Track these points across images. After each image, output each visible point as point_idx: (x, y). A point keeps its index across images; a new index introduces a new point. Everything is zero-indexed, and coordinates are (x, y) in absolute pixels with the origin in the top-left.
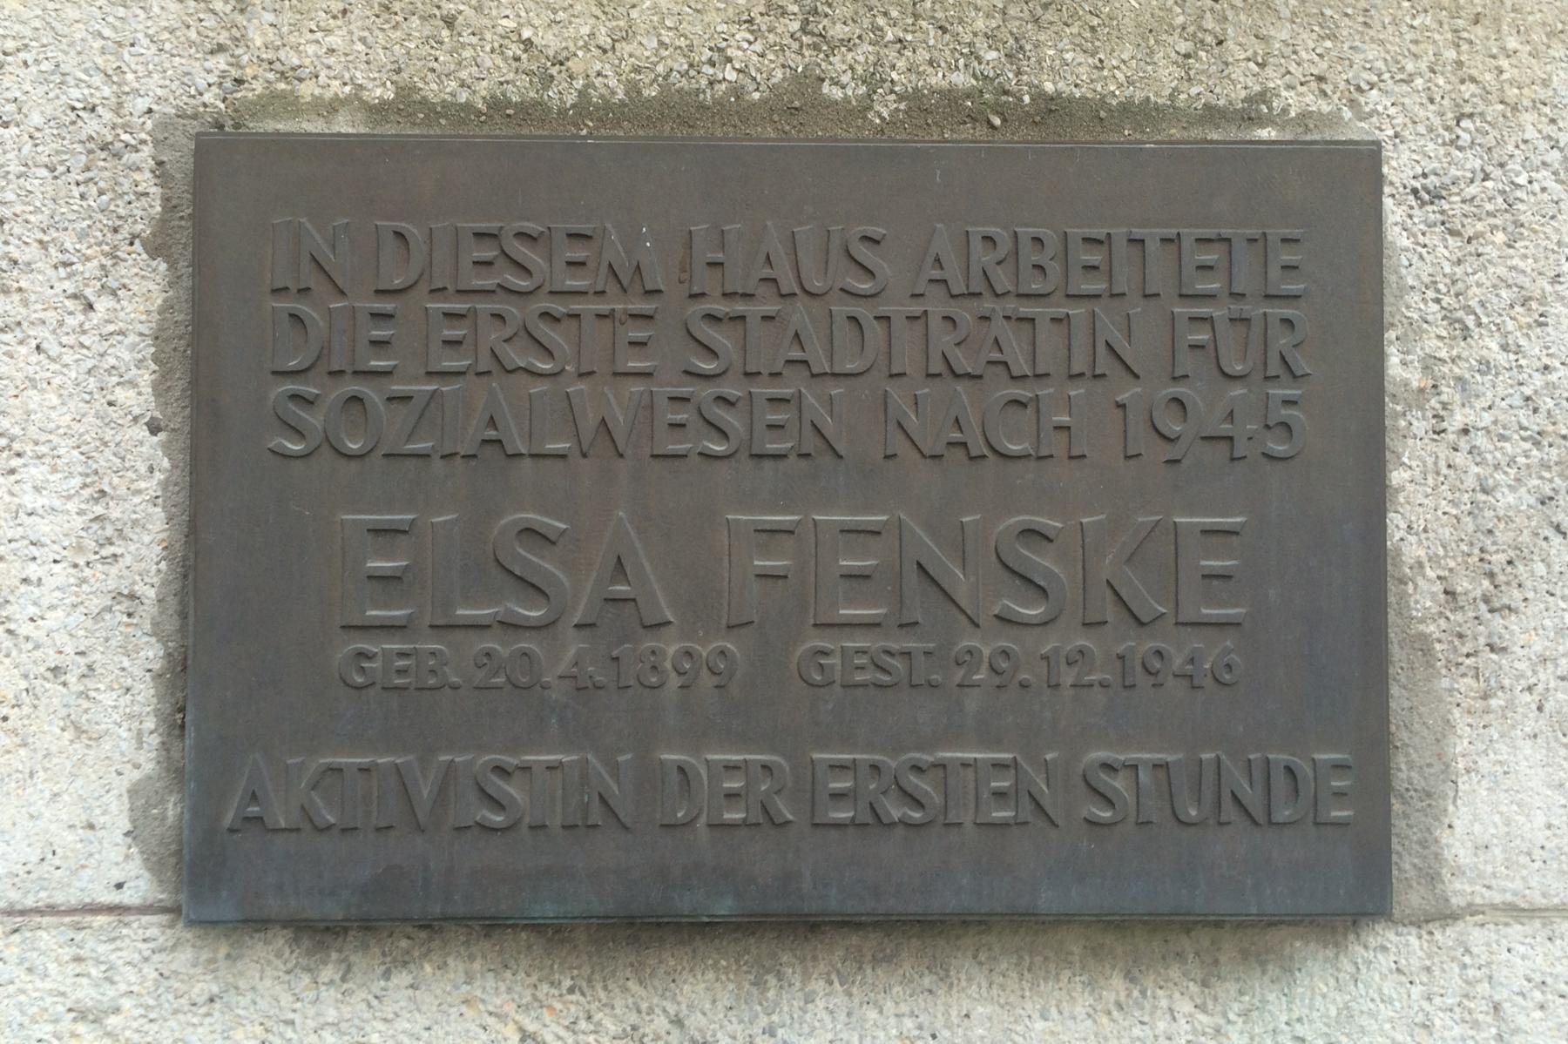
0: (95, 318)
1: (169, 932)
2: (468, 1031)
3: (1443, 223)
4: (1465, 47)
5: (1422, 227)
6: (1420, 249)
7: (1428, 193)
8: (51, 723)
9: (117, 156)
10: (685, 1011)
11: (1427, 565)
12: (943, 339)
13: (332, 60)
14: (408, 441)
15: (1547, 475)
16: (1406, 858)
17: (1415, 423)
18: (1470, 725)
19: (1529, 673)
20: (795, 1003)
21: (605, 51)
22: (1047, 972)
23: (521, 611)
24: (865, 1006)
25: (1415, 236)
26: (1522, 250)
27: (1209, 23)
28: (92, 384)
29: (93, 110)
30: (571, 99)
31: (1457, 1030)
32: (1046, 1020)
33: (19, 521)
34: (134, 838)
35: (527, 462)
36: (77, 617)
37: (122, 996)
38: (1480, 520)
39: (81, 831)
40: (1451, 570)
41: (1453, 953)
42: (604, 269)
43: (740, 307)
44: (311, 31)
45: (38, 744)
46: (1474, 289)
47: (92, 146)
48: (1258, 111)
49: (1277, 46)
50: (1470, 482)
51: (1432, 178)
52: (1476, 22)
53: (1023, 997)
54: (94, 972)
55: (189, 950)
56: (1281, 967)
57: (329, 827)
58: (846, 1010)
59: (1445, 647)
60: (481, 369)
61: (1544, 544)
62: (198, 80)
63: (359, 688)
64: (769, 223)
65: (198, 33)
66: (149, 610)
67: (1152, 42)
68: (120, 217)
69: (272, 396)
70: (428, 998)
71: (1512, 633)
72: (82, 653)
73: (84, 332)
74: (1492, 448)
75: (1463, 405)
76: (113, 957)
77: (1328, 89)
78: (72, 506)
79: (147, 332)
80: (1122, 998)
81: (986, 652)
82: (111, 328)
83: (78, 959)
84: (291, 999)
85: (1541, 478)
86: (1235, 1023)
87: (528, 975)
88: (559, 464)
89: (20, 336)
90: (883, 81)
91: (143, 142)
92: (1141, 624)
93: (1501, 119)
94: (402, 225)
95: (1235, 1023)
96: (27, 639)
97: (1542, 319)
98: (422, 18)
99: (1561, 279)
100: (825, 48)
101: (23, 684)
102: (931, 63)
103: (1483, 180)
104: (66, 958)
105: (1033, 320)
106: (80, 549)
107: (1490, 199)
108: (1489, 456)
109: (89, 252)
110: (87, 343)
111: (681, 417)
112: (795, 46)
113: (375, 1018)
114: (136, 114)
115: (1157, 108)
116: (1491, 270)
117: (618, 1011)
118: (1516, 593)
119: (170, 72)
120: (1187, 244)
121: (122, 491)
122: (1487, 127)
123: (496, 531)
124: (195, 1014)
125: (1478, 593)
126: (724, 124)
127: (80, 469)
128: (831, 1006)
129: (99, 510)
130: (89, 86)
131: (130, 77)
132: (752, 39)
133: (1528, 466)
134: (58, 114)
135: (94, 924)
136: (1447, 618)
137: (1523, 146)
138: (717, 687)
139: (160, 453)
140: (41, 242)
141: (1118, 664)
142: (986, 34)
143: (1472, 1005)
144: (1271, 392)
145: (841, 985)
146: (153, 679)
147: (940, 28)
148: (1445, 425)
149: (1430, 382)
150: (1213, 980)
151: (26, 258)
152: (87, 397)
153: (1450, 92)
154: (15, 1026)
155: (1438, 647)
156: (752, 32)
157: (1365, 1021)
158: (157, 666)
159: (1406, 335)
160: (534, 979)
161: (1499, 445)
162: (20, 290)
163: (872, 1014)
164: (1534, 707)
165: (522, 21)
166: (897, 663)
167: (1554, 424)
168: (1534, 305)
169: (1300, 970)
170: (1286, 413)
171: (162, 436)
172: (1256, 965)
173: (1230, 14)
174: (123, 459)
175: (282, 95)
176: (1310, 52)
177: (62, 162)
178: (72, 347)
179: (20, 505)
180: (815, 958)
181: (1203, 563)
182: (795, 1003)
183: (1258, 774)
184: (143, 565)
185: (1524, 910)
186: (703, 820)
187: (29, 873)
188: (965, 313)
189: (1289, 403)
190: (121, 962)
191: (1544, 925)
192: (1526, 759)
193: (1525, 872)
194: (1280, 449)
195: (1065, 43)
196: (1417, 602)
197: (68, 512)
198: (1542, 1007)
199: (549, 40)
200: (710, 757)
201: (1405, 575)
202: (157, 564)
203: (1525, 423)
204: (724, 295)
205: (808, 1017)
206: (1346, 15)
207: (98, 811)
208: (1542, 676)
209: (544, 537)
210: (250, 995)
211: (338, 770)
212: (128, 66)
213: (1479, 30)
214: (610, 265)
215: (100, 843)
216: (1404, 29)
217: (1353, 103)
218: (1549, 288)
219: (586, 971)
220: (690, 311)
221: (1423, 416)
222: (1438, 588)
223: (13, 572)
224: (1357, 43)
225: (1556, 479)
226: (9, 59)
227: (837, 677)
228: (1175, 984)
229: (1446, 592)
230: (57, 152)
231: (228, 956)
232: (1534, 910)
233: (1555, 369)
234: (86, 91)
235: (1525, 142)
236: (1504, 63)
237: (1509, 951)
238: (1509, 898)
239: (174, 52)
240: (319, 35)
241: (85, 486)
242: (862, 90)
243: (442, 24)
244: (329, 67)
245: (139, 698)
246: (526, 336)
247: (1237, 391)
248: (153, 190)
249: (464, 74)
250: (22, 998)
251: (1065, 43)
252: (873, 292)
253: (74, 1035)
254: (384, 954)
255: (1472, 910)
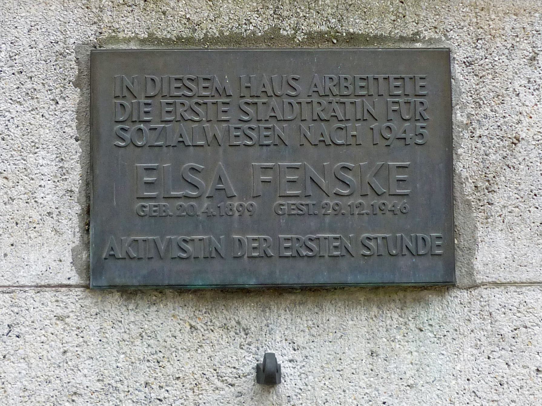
0: (59, 106)
1: (84, 293)
2: (174, 324)
3: (473, 72)
4: (479, 18)
5: (466, 73)
6: (466, 80)
7: (468, 63)
8: (48, 229)
9: (65, 57)
10: (241, 319)
11: (469, 178)
12: (318, 109)
13: (128, 26)
14: (156, 142)
15: (505, 150)
16: (463, 269)
17: (465, 134)
18: (482, 227)
19: (500, 211)
20: (275, 317)
21: (212, 21)
22: (353, 306)
23: (191, 193)
24: (297, 318)
25: (464, 76)
26: (497, 81)
27: (401, 10)
28: (58, 126)
29: (57, 43)
30: (202, 36)
31: (478, 321)
32: (353, 321)
33: (38, 168)
34: (73, 264)
35: (192, 148)
36: (55, 197)
37: (70, 312)
38: (485, 164)
39: (57, 262)
40: (476, 180)
41: (478, 297)
42: (214, 89)
43: (256, 100)
44: (122, 17)
45: (45, 235)
46: (482, 92)
47: (58, 54)
48: (416, 38)
49: (422, 17)
50: (482, 152)
51: (469, 58)
52: (482, 10)
53: (346, 314)
54: (62, 305)
55: (90, 298)
56: (425, 303)
57: (134, 258)
58: (290, 319)
59: (475, 203)
60: (177, 120)
61: (504, 171)
62: (89, 33)
63: (142, 216)
64: (264, 74)
65: (88, 19)
66: (76, 195)
67: (383, 16)
68: (66, 75)
69: (115, 129)
70: (162, 315)
71: (495, 199)
72: (57, 208)
73: (56, 111)
74: (488, 141)
75: (479, 128)
76: (67, 300)
77: (438, 31)
78: (53, 163)
79: (74, 110)
80: (376, 314)
81: (331, 204)
82: (64, 109)
83: (57, 301)
84: (121, 314)
85: (503, 151)
86: (411, 321)
87: (192, 308)
88: (201, 148)
89: (37, 112)
90: (299, 29)
91: (72, 52)
92: (379, 195)
93: (490, 40)
94: (153, 77)
95: (411, 321)
96: (41, 204)
97: (503, 102)
98: (156, 12)
99: (508, 89)
100: (281, 19)
101: (40, 217)
102: (314, 23)
103: (485, 59)
104: (54, 300)
105: (345, 103)
106: (56, 176)
107: (487, 65)
108: (487, 144)
109: (57, 86)
110: (57, 114)
111: (238, 134)
112: (272, 18)
113: (146, 320)
114: (70, 44)
115: (385, 37)
116: (487, 87)
117: (220, 319)
118: (496, 186)
119: (80, 31)
120: (391, 79)
121: (68, 159)
122: (486, 42)
123: (183, 168)
124: (92, 318)
125: (484, 187)
126: (250, 43)
127: (55, 152)
128: (286, 318)
129: (61, 165)
130: (56, 36)
131: (68, 32)
132: (258, 16)
133: (499, 147)
134: (47, 44)
135: (62, 290)
136: (475, 195)
137: (497, 49)
138: (250, 215)
139: (79, 147)
140: (43, 83)
141: (371, 207)
142: (331, 14)
143: (483, 313)
144: (417, 124)
145: (289, 311)
146: (78, 215)
147: (317, 12)
148: (474, 135)
149: (470, 122)
150: (405, 308)
151: (39, 88)
152: (57, 130)
153: (474, 32)
154: (39, 321)
155: (473, 203)
156: (258, 14)
157: (450, 319)
158: (79, 212)
159: (462, 107)
160: (194, 309)
161: (490, 140)
162: (37, 98)
163: (299, 320)
164: (502, 221)
165: (187, 12)
166: (304, 208)
167: (507, 134)
168: (500, 97)
169: (431, 304)
170: (422, 131)
171: (79, 142)
172: (417, 303)
173: (407, 8)
174: (68, 149)
175: (114, 37)
176: (432, 21)
177: (49, 59)
178: (52, 115)
179: (38, 163)
180: (281, 303)
181: (397, 176)
182: (275, 317)
183: (413, 239)
184: (75, 181)
185: (498, 284)
186: (246, 255)
187: (42, 274)
188: (324, 101)
189: (423, 127)
190: (70, 302)
191: (505, 288)
192: (499, 237)
193: (499, 272)
194: (420, 141)
195: (356, 17)
196: (466, 190)
197: (52, 165)
198: (505, 314)
199: (195, 18)
200: (248, 236)
201: (463, 181)
202: (79, 181)
203: (498, 134)
204: (251, 96)
205: (279, 321)
206: (443, 8)
207: (62, 256)
208: (504, 212)
209: (197, 170)
210: (108, 313)
211: (136, 241)
212: (68, 29)
213: (483, 13)
214: (216, 88)
215: (63, 265)
216: (461, 12)
217: (445, 35)
218: (505, 92)
219: (210, 307)
220: (241, 101)
221: (468, 132)
222: (473, 185)
223: (37, 183)
224: (446, 17)
225: (507, 151)
226: (33, 28)
227: (286, 212)
228: (393, 309)
229: (475, 187)
230: (48, 56)
231: (101, 301)
232: (501, 284)
233: (507, 117)
234: (55, 37)
235: (497, 47)
236: (491, 23)
237: (494, 296)
238: (494, 280)
239: (81, 25)
240: (125, 18)
241: (57, 157)
242: (293, 32)
243: (162, 14)
244: (128, 28)
245: (74, 222)
246: (191, 109)
247: (407, 124)
248: (75, 67)
249: (169, 29)
250: (40, 312)
251: (356, 17)
252: (296, 95)
253: (56, 324)
254: (148, 301)
255: (483, 284)
